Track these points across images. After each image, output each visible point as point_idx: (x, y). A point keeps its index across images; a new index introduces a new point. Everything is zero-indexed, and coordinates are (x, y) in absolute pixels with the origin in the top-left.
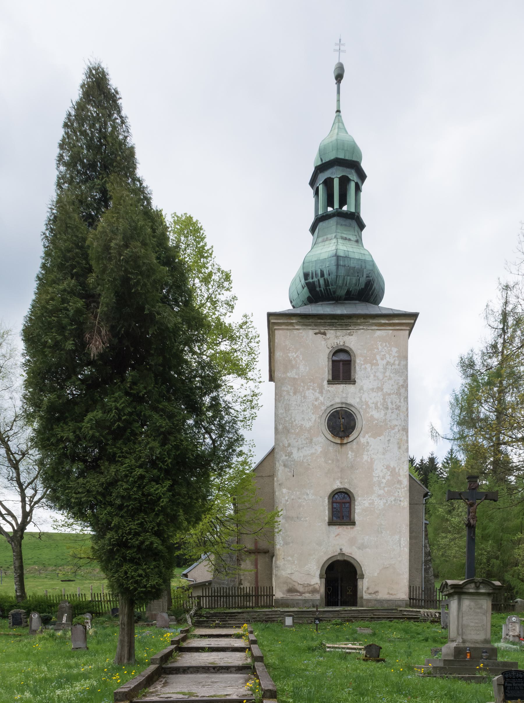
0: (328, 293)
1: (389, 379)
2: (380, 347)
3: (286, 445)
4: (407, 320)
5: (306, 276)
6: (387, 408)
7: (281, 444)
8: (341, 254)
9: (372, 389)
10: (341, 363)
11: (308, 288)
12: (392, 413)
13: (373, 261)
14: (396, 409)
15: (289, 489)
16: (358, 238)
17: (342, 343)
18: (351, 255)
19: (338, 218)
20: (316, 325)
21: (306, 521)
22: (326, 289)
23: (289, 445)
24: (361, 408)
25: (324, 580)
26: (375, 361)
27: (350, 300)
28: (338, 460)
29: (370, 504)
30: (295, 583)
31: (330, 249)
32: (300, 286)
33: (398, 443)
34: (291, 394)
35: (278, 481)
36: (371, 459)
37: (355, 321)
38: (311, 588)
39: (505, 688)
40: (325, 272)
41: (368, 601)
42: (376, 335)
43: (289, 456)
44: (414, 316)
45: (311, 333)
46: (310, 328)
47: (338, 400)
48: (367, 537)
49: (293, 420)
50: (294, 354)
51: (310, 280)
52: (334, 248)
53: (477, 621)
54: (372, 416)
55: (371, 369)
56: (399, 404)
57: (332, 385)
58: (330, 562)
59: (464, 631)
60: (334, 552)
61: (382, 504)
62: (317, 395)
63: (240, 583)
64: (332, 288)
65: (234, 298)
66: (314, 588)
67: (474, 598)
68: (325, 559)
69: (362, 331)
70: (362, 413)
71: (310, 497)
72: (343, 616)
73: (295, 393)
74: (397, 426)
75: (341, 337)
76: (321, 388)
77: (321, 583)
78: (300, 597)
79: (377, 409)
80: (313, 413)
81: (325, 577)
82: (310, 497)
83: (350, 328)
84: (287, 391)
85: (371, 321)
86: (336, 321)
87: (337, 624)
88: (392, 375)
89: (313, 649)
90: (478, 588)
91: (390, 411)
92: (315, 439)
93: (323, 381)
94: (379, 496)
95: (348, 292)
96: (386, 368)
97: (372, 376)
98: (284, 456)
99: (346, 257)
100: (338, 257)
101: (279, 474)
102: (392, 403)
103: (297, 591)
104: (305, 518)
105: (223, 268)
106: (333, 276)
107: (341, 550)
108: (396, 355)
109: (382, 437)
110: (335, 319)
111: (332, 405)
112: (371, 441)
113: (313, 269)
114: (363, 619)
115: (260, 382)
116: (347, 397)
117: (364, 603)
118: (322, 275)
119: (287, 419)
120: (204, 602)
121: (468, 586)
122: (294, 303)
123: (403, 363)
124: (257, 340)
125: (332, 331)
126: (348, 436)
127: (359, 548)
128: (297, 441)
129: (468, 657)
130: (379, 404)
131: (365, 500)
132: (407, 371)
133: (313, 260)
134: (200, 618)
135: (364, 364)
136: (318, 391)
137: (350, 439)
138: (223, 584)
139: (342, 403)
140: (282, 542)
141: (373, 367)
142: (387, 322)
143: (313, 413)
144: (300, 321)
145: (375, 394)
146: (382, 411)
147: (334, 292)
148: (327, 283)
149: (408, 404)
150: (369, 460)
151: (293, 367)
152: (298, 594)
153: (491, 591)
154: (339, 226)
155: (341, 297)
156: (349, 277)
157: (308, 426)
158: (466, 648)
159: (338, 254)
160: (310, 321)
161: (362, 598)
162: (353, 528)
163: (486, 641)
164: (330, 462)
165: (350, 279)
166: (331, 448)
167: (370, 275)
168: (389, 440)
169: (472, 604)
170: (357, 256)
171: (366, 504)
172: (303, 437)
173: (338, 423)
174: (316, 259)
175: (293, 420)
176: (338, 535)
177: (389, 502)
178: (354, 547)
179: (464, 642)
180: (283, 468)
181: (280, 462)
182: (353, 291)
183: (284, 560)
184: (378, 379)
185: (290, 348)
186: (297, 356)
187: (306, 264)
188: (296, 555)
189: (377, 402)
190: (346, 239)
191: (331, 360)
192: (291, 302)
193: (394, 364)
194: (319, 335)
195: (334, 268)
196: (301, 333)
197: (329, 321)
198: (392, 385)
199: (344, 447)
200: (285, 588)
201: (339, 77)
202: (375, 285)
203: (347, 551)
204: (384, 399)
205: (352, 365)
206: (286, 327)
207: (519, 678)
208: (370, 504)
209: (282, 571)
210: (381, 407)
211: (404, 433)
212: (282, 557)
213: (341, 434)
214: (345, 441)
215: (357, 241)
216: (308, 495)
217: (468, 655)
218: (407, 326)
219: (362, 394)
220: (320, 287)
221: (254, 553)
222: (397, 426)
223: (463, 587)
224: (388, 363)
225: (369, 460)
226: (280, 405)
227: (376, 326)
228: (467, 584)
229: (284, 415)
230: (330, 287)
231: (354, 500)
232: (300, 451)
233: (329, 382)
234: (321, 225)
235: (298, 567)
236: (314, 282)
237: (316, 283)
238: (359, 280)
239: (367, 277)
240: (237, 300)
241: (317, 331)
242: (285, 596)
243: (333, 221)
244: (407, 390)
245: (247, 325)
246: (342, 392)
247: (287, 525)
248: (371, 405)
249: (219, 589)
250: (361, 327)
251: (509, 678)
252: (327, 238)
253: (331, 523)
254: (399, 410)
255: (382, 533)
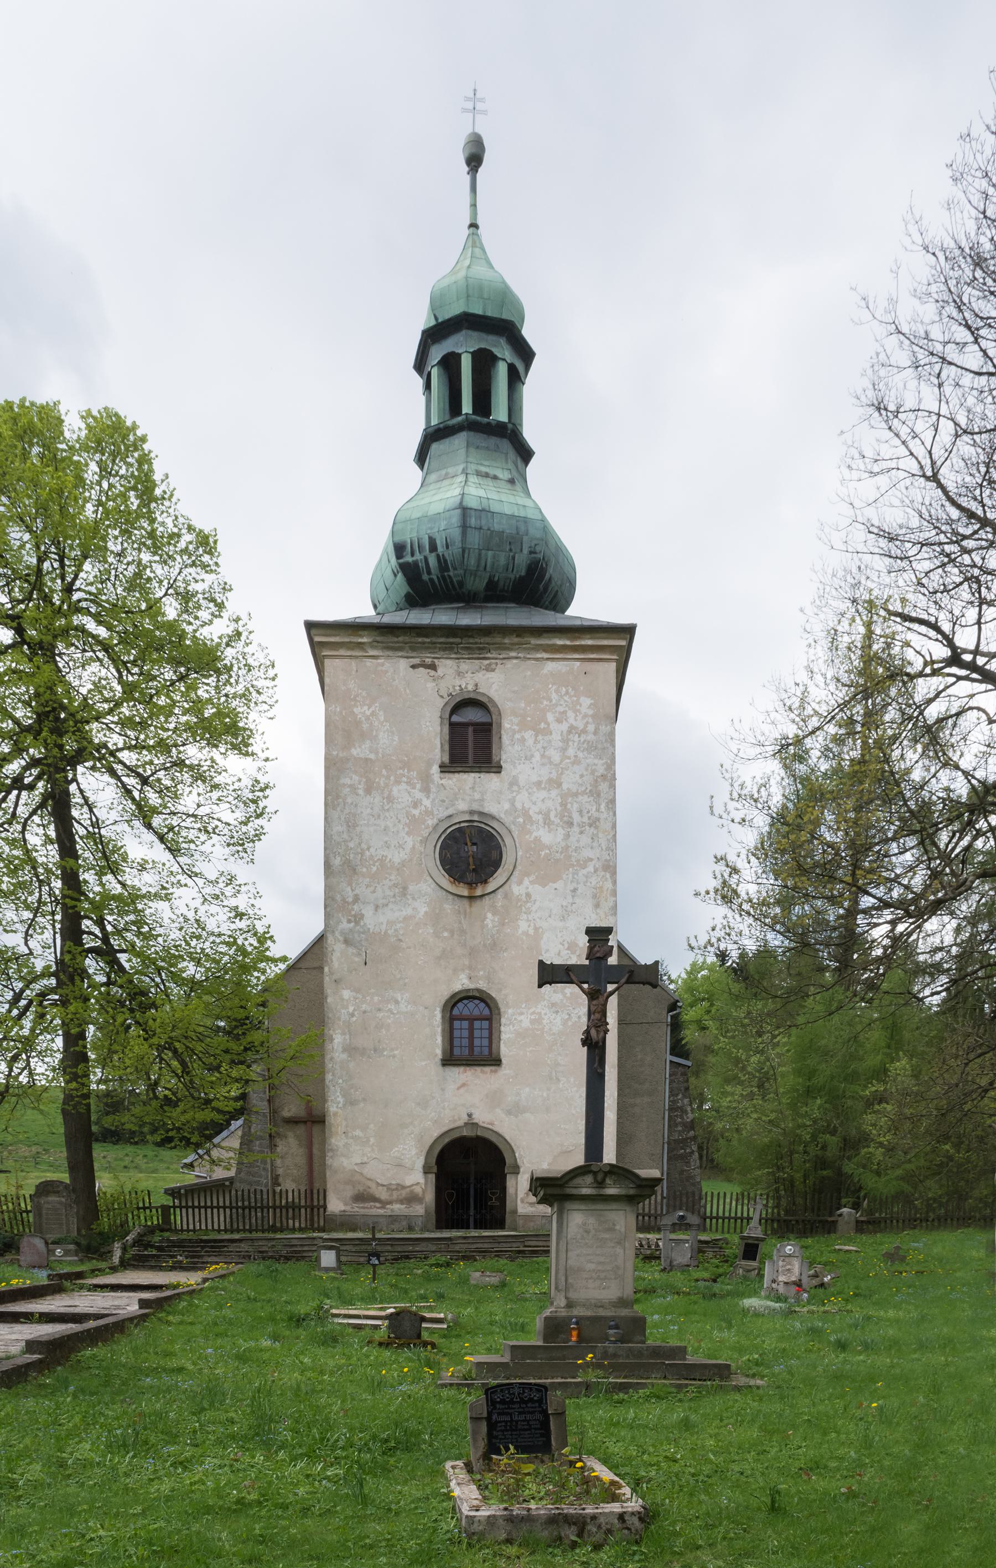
0: (447, 585)
1: (573, 763)
2: (554, 696)
3: (350, 900)
4: (616, 640)
5: (399, 549)
6: (570, 824)
7: (338, 898)
8: (472, 503)
9: (539, 784)
10: (471, 729)
11: (405, 575)
12: (581, 833)
13: (543, 520)
14: (590, 826)
15: (357, 990)
16: (515, 474)
17: (470, 688)
18: (495, 507)
19: (472, 433)
20: (413, 649)
21: (394, 1056)
22: (443, 577)
23: (356, 899)
24: (514, 823)
25: (432, 1177)
26: (543, 725)
27: (498, 602)
28: (463, 932)
29: (532, 1022)
30: (369, 1183)
31: (449, 494)
32: (389, 573)
33: (594, 896)
34: (361, 792)
35: (331, 973)
36: (536, 929)
37: (498, 640)
38: (404, 1193)
39: (491, 1426)
40: (438, 542)
41: (528, 1218)
42: (545, 671)
43: (357, 923)
44: (628, 631)
45: (403, 664)
46: (400, 654)
47: (462, 806)
48: (527, 1090)
49: (364, 846)
50: (366, 708)
51: (409, 559)
52: (457, 491)
53: (602, 1259)
54: (537, 840)
55: (536, 742)
56: (596, 815)
57: (451, 775)
58: (447, 1140)
59: (570, 1281)
60: (455, 1121)
61: (558, 1021)
62: (418, 795)
63: (276, 1182)
64: (456, 576)
65: (226, 588)
66: (412, 1192)
67: (593, 1207)
68: (436, 1134)
69: (515, 661)
70: (515, 834)
71: (403, 1007)
72: (457, 1248)
73: (368, 791)
74: (591, 860)
75: (469, 674)
76: (426, 780)
77: (426, 1184)
78: (381, 1212)
79: (549, 825)
80: (408, 833)
81: (435, 1170)
82: (403, 1007)
83: (489, 655)
84: (350, 786)
85: (534, 641)
86: (458, 640)
87: (437, 1265)
88: (580, 755)
89: (298, 1321)
90: (600, 1184)
91: (576, 829)
92: (412, 888)
93: (429, 765)
94: (553, 1005)
95: (492, 585)
96: (568, 740)
97: (537, 756)
98: (344, 921)
99: (483, 510)
100: (465, 511)
101: (334, 959)
102: (580, 812)
103: (375, 1200)
104: (392, 1050)
105: (198, 525)
106: (456, 549)
107: (470, 1115)
108: (590, 712)
109: (559, 885)
110: (455, 636)
111: (450, 816)
112: (536, 890)
113: (414, 535)
114: (499, 1254)
115: (267, 760)
116: (483, 800)
117: (520, 1222)
118: (433, 547)
119: (351, 845)
120: (216, 1220)
121: (579, 1181)
122: (380, 609)
123: (604, 729)
124: (271, 673)
125: (449, 662)
126: (485, 882)
127: (509, 1113)
128: (374, 892)
129: (574, 1339)
130: (552, 814)
131: (522, 1014)
132: (614, 746)
133: (414, 516)
134: (146, 1249)
135: (519, 731)
136: (418, 786)
137: (491, 886)
138: (258, 1183)
139: (472, 812)
140: (341, 1099)
141: (540, 737)
142: (568, 643)
143: (408, 833)
144: (378, 639)
145: (543, 794)
146: (560, 829)
147: (461, 584)
148: (443, 564)
149: (615, 814)
150: (531, 932)
151: (363, 736)
152: (378, 1205)
153: (632, 1192)
154: (472, 450)
155: (479, 593)
156: (490, 553)
157: (397, 860)
158: (571, 1317)
159: (464, 504)
160: (401, 639)
161: (515, 1211)
162: (496, 1071)
163: (622, 1302)
164: (446, 934)
165: (494, 557)
166: (448, 907)
167: (538, 549)
168: (575, 890)
169: (592, 1221)
170: (507, 510)
171: (525, 1021)
172: (387, 882)
173: (463, 854)
174: (419, 515)
175: (364, 846)
176: (463, 1085)
177: (575, 1019)
178: (498, 1111)
179: (570, 1305)
180: (343, 946)
181: (337, 934)
182: (501, 583)
183: (347, 1137)
184: (551, 763)
185: (357, 696)
186: (373, 714)
187: (398, 527)
188: (372, 1126)
189: (549, 811)
190: (487, 475)
191: (447, 722)
192: (375, 607)
193: (584, 731)
194: (421, 669)
195: (456, 533)
196: (383, 665)
197: (442, 640)
198: (582, 776)
199: (478, 903)
200: (349, 1192)
201: (475, 161)
202: (550, 571)
203: (483, 1117)
204: (563, 805)
205: (494, 732)
206: (349, 653)
207: (531, 1400)
208: (532, 1022)
209: (343, 1159)
210: (557, 821)
211: (608, 875)
212: (340, 1130)
213: (470, 877)
214: (479, 892)
215: (512, 481)
216: (397, 1002)
217: (575, 1333)
218: (612, 653)
219: (512, 795)
220: (429, 573)
221: (305, 1122)
222: (591, 860)
223: (567, 1182)
224: (572, 729)
225: (531, 932)
226: (335, 814)
227: (545, 651)
228: (572, 1179)
229: (345, 836)
230: (451, 574)
231: (499, 1014)
232: (380, 911)
233: (444, 769)
234: (435, 447)
235: (380, 1148)
236: (416, 563)
237: (422, 565)
238: (514, 558)
239: (531, 553)
240: (231, 590)
241: (417, 661)
242: (348, 1208)
243: (460, 440)
244: (613, 786)
245: (243, 638)
246: (473, 788)
247: (352, 1065)
248: (535, 817)
249: (246, 1193)
250: (513, 654)
251: (503, 1402)
252: (447, 474)
253: (450, 1060)
254: (596, 828)
255: (558, 1080)
